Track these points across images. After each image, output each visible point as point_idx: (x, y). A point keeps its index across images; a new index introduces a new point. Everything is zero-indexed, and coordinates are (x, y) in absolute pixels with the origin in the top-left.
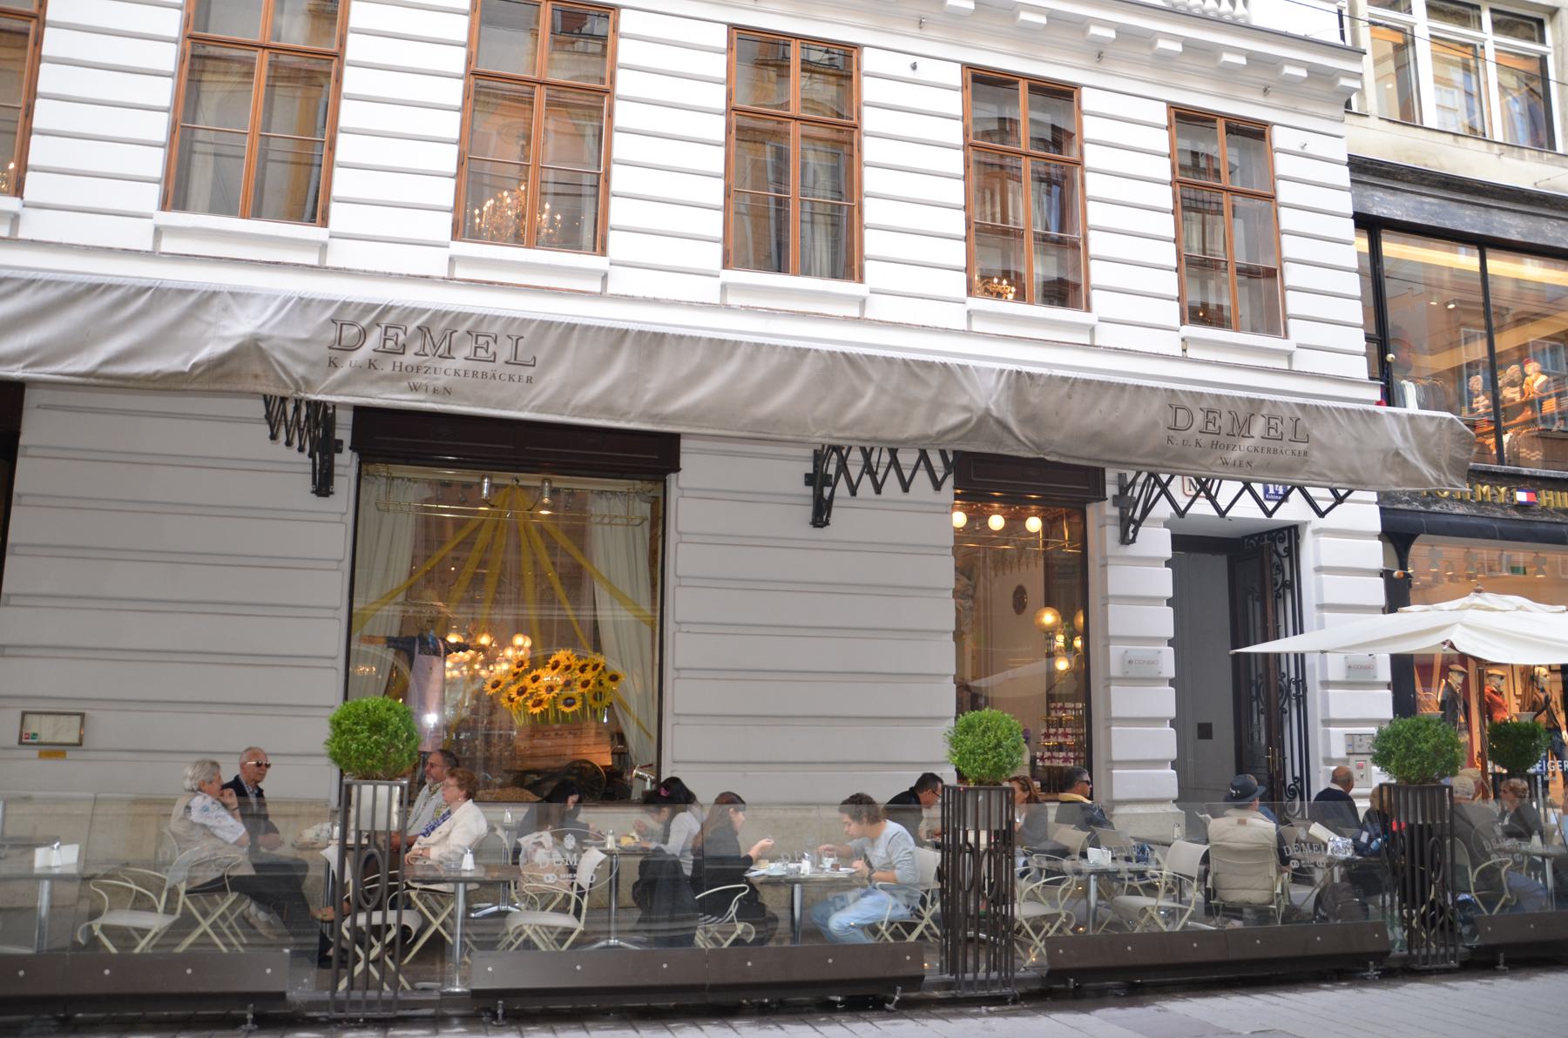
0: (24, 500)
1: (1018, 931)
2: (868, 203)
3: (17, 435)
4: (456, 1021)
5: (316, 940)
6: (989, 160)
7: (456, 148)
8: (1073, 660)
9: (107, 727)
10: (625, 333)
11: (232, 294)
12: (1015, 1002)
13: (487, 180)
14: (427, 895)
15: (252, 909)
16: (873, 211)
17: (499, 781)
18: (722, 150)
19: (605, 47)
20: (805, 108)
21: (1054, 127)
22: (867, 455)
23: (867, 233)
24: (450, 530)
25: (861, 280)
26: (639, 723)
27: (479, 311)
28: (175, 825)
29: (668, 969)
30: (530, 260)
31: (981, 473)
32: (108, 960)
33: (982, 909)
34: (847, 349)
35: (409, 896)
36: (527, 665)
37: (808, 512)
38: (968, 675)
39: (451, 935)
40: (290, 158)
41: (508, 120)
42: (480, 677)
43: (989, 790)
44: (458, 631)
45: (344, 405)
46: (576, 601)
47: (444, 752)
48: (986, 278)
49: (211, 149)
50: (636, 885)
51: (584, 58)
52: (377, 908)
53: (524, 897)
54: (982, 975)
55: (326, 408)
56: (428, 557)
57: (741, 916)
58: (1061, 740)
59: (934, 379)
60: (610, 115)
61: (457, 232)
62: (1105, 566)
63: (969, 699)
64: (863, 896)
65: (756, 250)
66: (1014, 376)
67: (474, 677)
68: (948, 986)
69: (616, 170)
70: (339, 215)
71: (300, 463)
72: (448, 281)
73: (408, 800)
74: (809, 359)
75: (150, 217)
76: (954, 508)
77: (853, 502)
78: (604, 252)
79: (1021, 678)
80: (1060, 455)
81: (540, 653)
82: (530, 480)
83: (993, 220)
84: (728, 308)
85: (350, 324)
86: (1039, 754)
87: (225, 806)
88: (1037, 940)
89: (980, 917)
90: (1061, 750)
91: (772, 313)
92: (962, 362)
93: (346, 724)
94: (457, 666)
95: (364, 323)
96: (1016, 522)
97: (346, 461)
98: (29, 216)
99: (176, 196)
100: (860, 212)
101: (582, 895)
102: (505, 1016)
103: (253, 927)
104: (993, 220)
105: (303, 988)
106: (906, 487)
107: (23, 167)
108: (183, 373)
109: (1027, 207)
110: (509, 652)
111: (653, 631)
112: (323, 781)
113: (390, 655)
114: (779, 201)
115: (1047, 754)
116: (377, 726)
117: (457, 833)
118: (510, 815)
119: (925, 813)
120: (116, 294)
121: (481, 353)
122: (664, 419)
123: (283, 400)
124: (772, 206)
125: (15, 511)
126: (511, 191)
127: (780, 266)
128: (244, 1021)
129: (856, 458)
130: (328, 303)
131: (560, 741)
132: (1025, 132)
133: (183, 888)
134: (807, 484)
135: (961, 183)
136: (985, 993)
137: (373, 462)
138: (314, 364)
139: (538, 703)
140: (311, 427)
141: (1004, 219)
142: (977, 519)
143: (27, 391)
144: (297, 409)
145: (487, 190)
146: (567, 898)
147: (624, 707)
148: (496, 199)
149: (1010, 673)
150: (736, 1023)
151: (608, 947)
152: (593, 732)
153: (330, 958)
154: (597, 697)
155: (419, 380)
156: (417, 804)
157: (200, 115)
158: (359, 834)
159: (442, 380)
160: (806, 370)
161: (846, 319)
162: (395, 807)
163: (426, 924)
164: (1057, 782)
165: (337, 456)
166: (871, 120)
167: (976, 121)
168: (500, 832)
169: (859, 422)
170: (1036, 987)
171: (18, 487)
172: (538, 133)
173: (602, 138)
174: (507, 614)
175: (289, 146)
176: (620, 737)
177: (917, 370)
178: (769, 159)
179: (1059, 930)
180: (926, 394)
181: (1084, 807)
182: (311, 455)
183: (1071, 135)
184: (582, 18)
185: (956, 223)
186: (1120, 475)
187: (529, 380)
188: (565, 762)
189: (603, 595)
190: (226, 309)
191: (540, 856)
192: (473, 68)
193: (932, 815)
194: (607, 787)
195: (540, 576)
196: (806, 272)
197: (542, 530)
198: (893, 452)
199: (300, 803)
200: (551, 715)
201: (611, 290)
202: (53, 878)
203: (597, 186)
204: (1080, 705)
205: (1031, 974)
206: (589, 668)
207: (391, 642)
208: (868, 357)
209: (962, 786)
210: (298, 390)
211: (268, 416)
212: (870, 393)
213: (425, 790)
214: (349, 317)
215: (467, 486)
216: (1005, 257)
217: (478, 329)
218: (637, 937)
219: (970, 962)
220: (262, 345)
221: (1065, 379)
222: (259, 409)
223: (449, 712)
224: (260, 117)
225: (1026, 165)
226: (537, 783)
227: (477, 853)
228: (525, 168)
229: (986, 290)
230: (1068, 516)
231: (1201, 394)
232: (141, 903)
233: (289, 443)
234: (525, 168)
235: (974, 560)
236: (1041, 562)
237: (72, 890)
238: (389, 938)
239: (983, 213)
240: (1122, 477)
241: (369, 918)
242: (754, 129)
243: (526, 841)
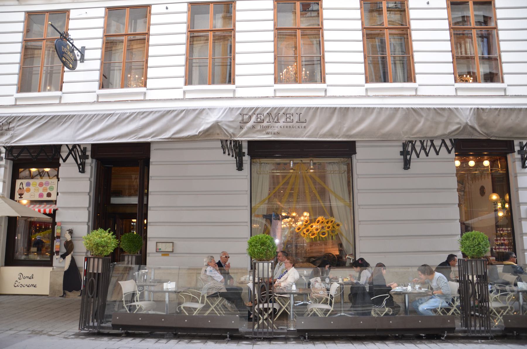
0: (153, 178)
1: (491, 313)
2: (415, 54)
3: (149, 159)
4: (292, 339)
5: (247, 313)
6: (458, 33)
7: (273, 54)
8: (505, 212)
9: (180, 246)
10: (335, 109)
11: (209, 109)
12: (492, 339)
13: (283, 63)
14: (281, 298)
15: (226, 302)
16: (417, 57)
17: (300, 261)
18: (362, 43)
19: (318, 13)
20: (389, 24)
21: (484, 17)
22: (422, 143)
23: (416, 65)
24: (281, 179)
25: (415, 82)
26: (346, 239)
27: (286, 106)
28: (202, 276)
29: (362, 323)
31: (465, 146)
32: (185, 317)
33: (476, 304)
34: (413, 107)
35: (275, 299)
36: (309, 222)
37: (402, 164)
38: (464, 219)
39: (289, 311)
40: (220, 64)
41: (288, 43)
42: (293, 227)
43: (476, 261)
44: (284, 212)
45: (245, 141)
46: (324, 200)
47: (283, 252)
48: (461, 76)
49: (198, 65)
50: (350, 295)
51: (311, 18)
52: (266, 302)
53: (312, 299)
54: (478, 328)
55: (239, 142)
56: (274, 188)
57: (387, 305)
58: (502, 242)
59: (446, 114)
60: (323, 36)
61: (276, 81)
62: (516, 177)
63: (465, 228)
64: (431, 298)
65: (375, 76)
66: (476, 110)
67: (291, 227)
68: (465, 332)
69: (326, 54)
70: (238, 80)
71: (232, 160)
72: (274, 97)
73: (273, 268)
74: (400, 112)
75: (12, 96)
76: (455, 159)
77: (418, 160)
78: (325, 82)
79: (484, 219)
80: (496, 137)
81: (313, 218)
82: (306, 160)
83: (461, 54)
84: (369, 96)
85: (245, 115)
86: (494, 247)
87: (216, 270)
88: (499, 316)
89: (476, 307)
90: (502, 246)
91: (384, 97)
92: (456, 107)
93: (253, 243)
94: (285, 223)
95: (250, 114)
96: (479, 163)
97: (246, 159)
98: (149, 92)
99: (189, 81)
100: (413, 58)
101: (332, 298)
102: (308, 338)
103: (226, 308)
104: (461, 54)
105: (244, 327)
106: (437, 153)
107: (146, 78)
108: (196, 135)
109: (475, 48)
110: (302, 218)
111: (350, 209)
112: (245, 261)
113: (264, 221)
115: (497, 247)
116: (263, 244)
117: (290, 278)
118: (306, 272)
119: (452, 269)
120: (175, 113)
121: (288, 120)
122: (350, 136)
123: (226, 141)
124: (380, 60)
125: (150, 181)
126: (291, 65)
127: (385, 80)
128: (227, 337)
129: (418, 144)
130: (239, 108)
131: (321, 247)
132: (472, 20)
133: (206, 296)
134: (401, 155)
135: (449, 42)
136: (479, 335)
137: (255, 159)
138: (235, 128)
139: (313, 234)
140: (235, 148)
141: (466, 53)
142: (465, 162)
143: (151, 145)
144: (231, 143)
145: (283, 66)
146: (327, 299)
147: (341, 234)
148: (287, 69)
149: (480, 218)
150: (387, 342)
151: (341, 316)
152: (331, 243)
153: (252, 318)
154: (333, 231)
155: (269, 130)
156: (276, 269)
157: (113, 59)
158: (259, 278)
159: (276, 130)
160: (399, 115)
161: (411, 96)
162: (270, 270)
163: (281, 308)
164: (502, 258)
165: (244, 157)
166: (414, 25)
167: (453, 19)
168: (303, 277)
169: (419, 131)
170: (500, 334)
171: (150, 175)
172: (300, 47)
173: (320, 44)
174: (300, 206)
175: (220, 60)
176: (341, 245)
177: (439, 111)
178: (377, 44)
179: (507, 313)
180: (443, 120)
181: (513, 267)
182: (236, 158)
183: (490, 18)
184: (309, 5)
185: (449, 57)
186: (520, 143)
187: (305, 127)
188: (323, 254)
189: (333, 198)
190: (207, 114)
191: (317, 285)
192: (276, 27)
193: (455, 270)
194: (338, 262)
195: (311, 192)
196: (395, 81)
197: (311, 177)
198: (432, 141)
199: (238, 269)
200: (318, 238)
201: (328, 94)
202: (169, 292)
203: (320, 60)
204: (509, 229)
205: (497, 329)
206: (330, 222)
207: (264, 216)
208: (421, 108)
209: (466, 259)
210: (231, 137)
211: (222, 146)
212: (422, 121)
213: (278, 264)
214: (245, 112)
215: (285, 164)
216: (468, 67)
217: (286, 112)
218: (350, 313)
219: (473, 323)
220: (219, 124)
221: (496, 109)
222: (219, 144)
223: (283, 238)
224: (211, 53)
225: (474, 32)
226: (314, 261)
227: (296, 284)
228: (296, 58)
229: (461, 80)
230: (500, 160)
231: (521, 109)
232: (194, 300)
233: (229, 154)
234: (296, 58)
235: (464, 177)
236: (490, 177)
237: (174, 296)
238: (270, 312)
239: (457, 53)
240: (521, 143)
241: (263, 306)
242: (371, 34)
243: (312, 280)
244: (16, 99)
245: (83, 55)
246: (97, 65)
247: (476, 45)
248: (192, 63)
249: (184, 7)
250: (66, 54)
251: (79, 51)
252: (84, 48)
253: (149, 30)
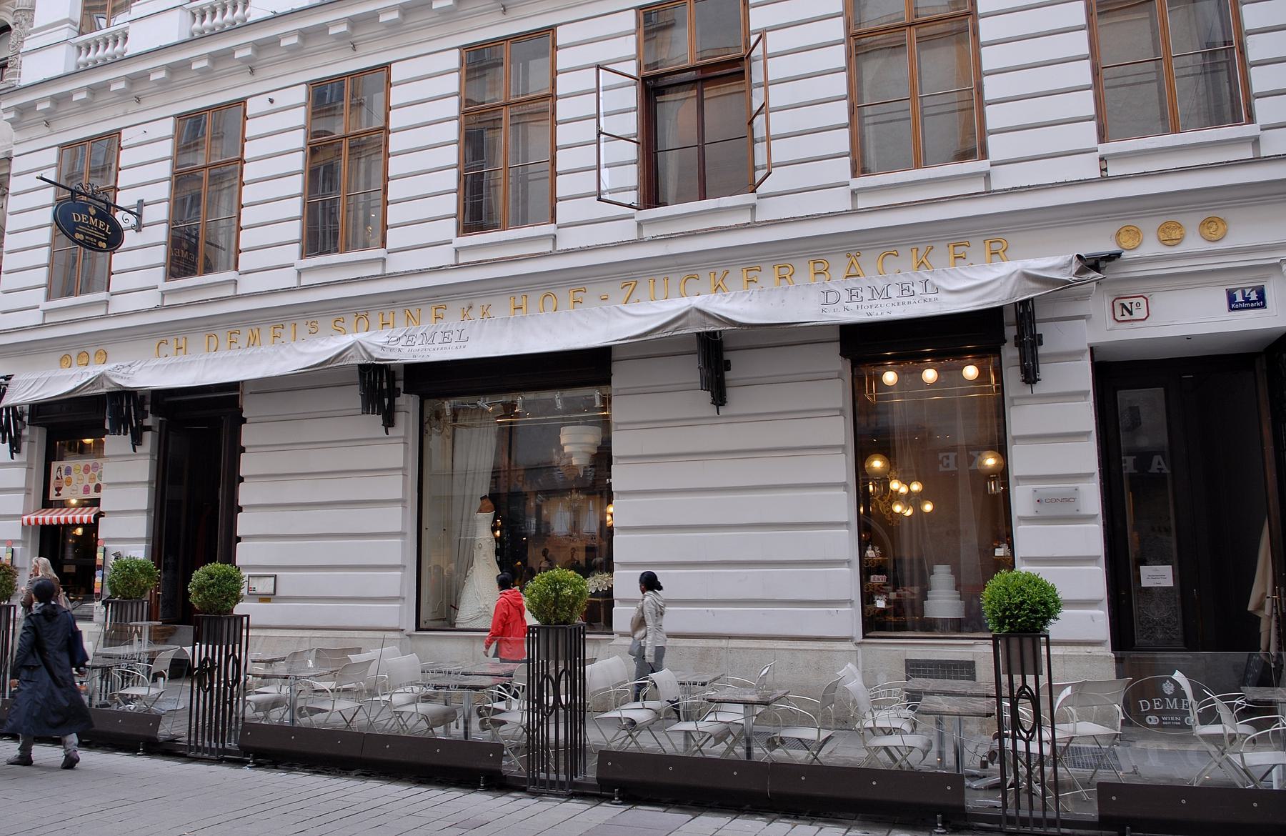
30: (1154, 146)
244: (163, 294)
249: (629, 21)
252: (141, 204)
253: (387, 119)
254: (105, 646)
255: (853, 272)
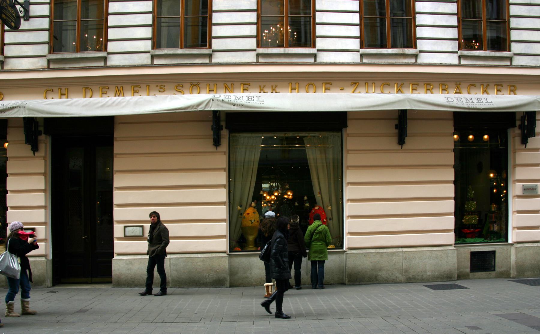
49: (167, 24)
61: (259, 44)
97: (225, 133)
114: (381, 20)
245: (27, 11)
246: (45, 23)
247: (484, 17)
248: (161, 23)
250: (6, 10)
251: (22, 6)
254: (494, 252)
255: (458, 91)
